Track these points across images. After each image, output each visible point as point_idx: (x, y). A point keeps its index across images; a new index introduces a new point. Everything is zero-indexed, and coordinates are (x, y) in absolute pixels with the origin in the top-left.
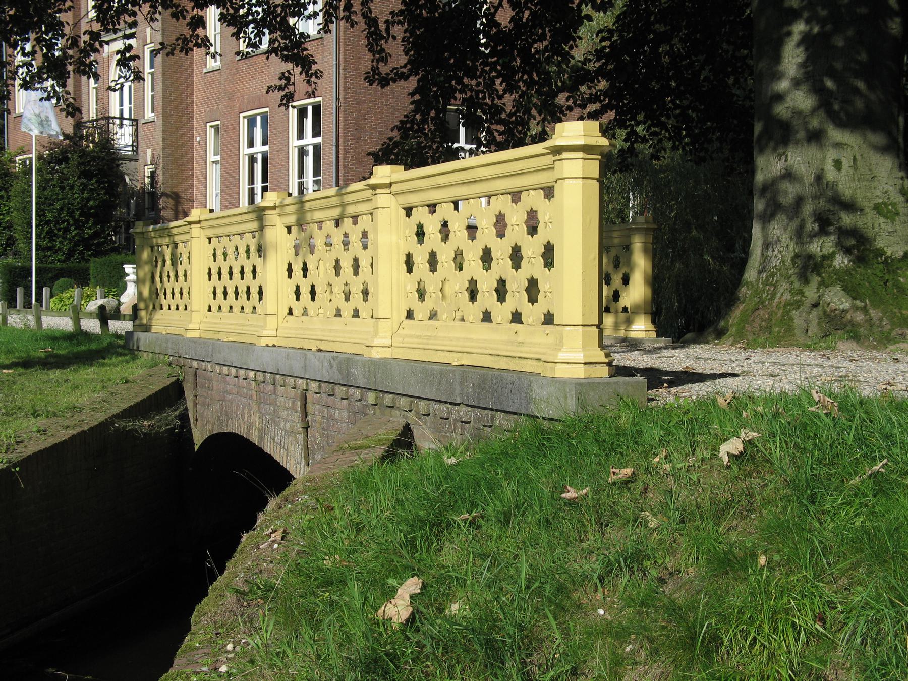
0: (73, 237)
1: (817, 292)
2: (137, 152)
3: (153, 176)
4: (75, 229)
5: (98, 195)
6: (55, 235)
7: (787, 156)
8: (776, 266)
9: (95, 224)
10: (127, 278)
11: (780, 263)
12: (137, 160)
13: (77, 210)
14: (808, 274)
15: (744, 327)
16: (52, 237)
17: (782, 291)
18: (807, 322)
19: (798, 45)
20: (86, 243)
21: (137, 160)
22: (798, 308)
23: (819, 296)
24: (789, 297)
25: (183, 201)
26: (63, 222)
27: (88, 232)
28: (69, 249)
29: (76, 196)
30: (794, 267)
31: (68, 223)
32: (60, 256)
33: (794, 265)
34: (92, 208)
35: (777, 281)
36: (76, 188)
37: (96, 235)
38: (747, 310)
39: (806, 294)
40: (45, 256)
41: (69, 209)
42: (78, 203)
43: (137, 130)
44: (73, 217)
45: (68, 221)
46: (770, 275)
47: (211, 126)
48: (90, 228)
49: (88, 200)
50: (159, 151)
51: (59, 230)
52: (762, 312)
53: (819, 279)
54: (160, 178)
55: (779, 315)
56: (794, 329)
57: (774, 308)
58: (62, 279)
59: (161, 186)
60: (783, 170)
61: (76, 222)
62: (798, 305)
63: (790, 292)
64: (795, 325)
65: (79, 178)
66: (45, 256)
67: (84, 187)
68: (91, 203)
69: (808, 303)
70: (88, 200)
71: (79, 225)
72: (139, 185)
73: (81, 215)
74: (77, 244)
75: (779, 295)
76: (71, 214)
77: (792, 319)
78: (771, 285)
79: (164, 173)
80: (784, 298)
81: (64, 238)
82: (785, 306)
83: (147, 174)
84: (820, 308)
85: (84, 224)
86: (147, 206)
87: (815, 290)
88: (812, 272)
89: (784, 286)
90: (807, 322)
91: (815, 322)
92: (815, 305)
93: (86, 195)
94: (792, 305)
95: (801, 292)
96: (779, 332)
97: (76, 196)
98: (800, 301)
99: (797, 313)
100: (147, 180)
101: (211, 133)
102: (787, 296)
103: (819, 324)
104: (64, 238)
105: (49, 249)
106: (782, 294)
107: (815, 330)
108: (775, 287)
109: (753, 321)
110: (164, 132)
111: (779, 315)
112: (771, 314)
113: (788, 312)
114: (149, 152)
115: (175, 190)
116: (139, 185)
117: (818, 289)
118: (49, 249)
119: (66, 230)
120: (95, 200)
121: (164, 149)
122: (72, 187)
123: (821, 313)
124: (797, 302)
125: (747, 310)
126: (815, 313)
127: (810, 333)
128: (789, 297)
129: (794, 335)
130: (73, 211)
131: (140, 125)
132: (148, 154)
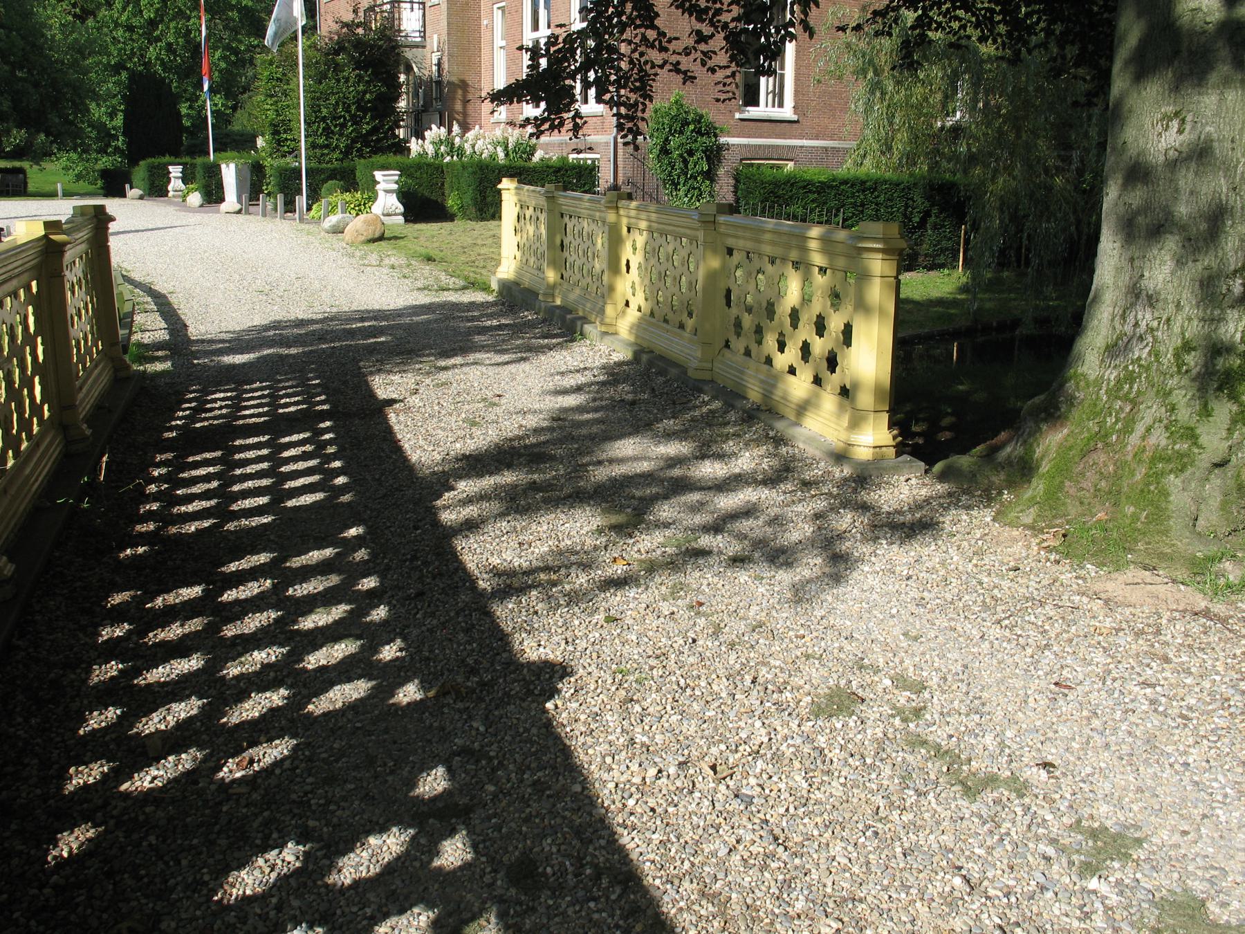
0: (351, 133)
1: (1227, 439)
2: (424, 37)
3: (439, 65)
4: (352, 125)
5: (375, 86)
6: (333, 132)
7: (1183, 121)
8: (1139, 358)
9: (373, 118)
10: (378, 187)
11: (1150, 354)
12: (424, 47)
13: (354, 104)
14: (1119, 84)
15: (1060, 487)
16: (328, 133)
17: (1148, 420)
18: (1199, 501)
19: (74, 208)
20: (365, 139)
21: (424, 47)
22: (1182, 471)
23: (1230, 447)
24: (1164, 442)
25: (470, 89)
26: (340, 117)
27: (366, 128)
28: (347, 146)
29: (351, 89)
30: (1179, 372)
31: (345, 119)
32: (336, 155)
33: (1179, 367)
34: (369, 101)
35: (1139, 392)
36: (351, 80)
37: (375, 130)
38: (1070, 448)
39: (1203, 440)
40: (323, 155)
41: (344, 103)
42: (354, 97)
43: (424, 15)
44: (349, 112)
45: (344, 116)
46: (1126, 379)
47: (499, 8)
48: (368, 123)
49: (365, 93)
50: (445, 37)
51: (336, 126)
52: (1101, 457)
53: (1235, 408)
54: (446, 66)
55: (1138, 477)
56: (1169, 517)
57: (1129, 458)
58: (330, 182)
59: (446, 77)
60: (1171, 152)
61: (353, 117)
62: (1181, 463)
63: (1167, 428)
64: (1171, 507)
65: (353, 70)
66: (323, 155)
67: (360, 77)
68: (368, 96)
69: (1204, 460)
70: (365, 93)
71: (356, 121)
72: (427, 73)
73: (358, 109)
74: (354, 141)
75: (1140, 428)
76: (347, 109)
77: (1165, 494)
78: (1126, 398)
79: (449, 61)
80: (1152, 440)
81: (341, 135)
82: (1153, 460)
83: (435, 61)
84: (1230, 471)
85: (361, 119)
86: (434, 96)
87: (1224, 434)
88: (1220, 389)
89: (1151, 411)
90: (1199, 501)
91: (1215, 502)
92: (1221, 464)
93: (361, 88)
94: (1169, 460)
95: (1191, 435)
96: (1135, 518)
97: (351, 89)
98: (1187, 455)
99: (1178, 482)
100: (435, 68)
101: (498, 15)
102: (1159, 438)
103: (1224, 506)
104: (341, 135)
105: (327, 146)
106: (1148, 430)
107: (1214, 518)
108: (1135, 403)
109: (1082, 474)
110: (449, 15)
111: (1138, 477)
112: (1121, 465)
113: (1160, 475)
114: (435, 37)
115: (462, 77)
116: (427, 73)
117: (1230, 431)
118: (327, 146)
119: (343, 126)
120: (371, 93)
121: (449, 34)
122: (347, 80)
123: (1231, 483)
124: (1181, 455)
125: (1070, 448)
126: (1216, 480)
127: (1201, 522)
128: (1164, 442)
129: (1166, 532)
130: (349, 106)
131: (427, 8)
132: (434, 41)
